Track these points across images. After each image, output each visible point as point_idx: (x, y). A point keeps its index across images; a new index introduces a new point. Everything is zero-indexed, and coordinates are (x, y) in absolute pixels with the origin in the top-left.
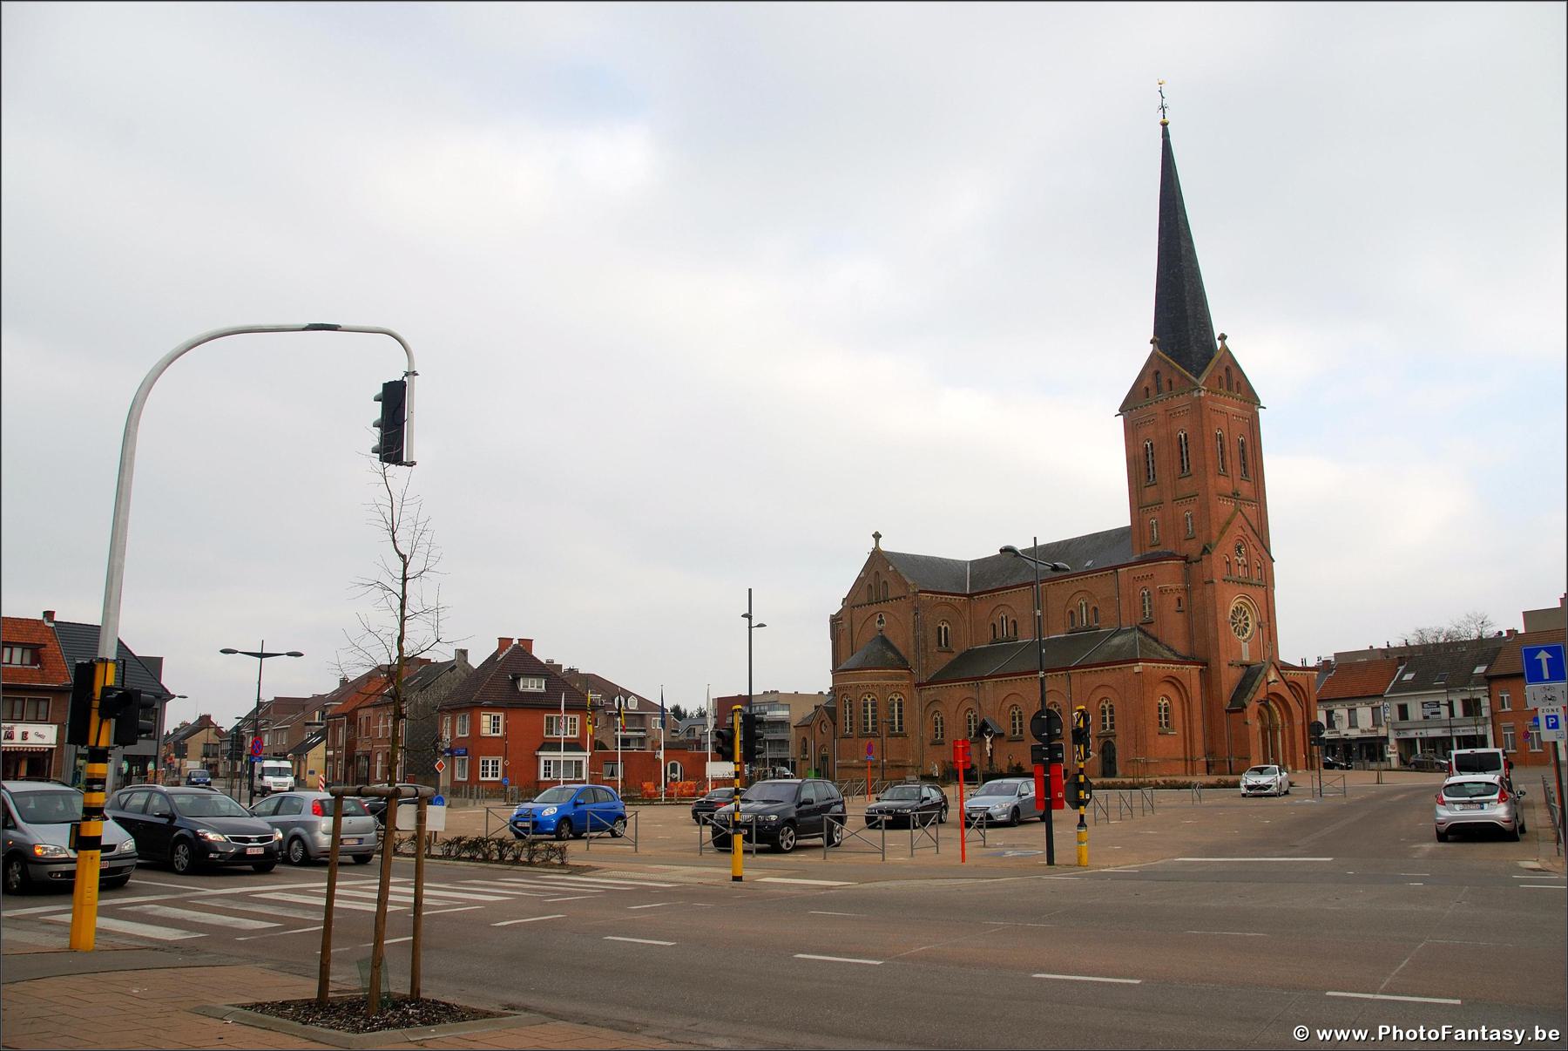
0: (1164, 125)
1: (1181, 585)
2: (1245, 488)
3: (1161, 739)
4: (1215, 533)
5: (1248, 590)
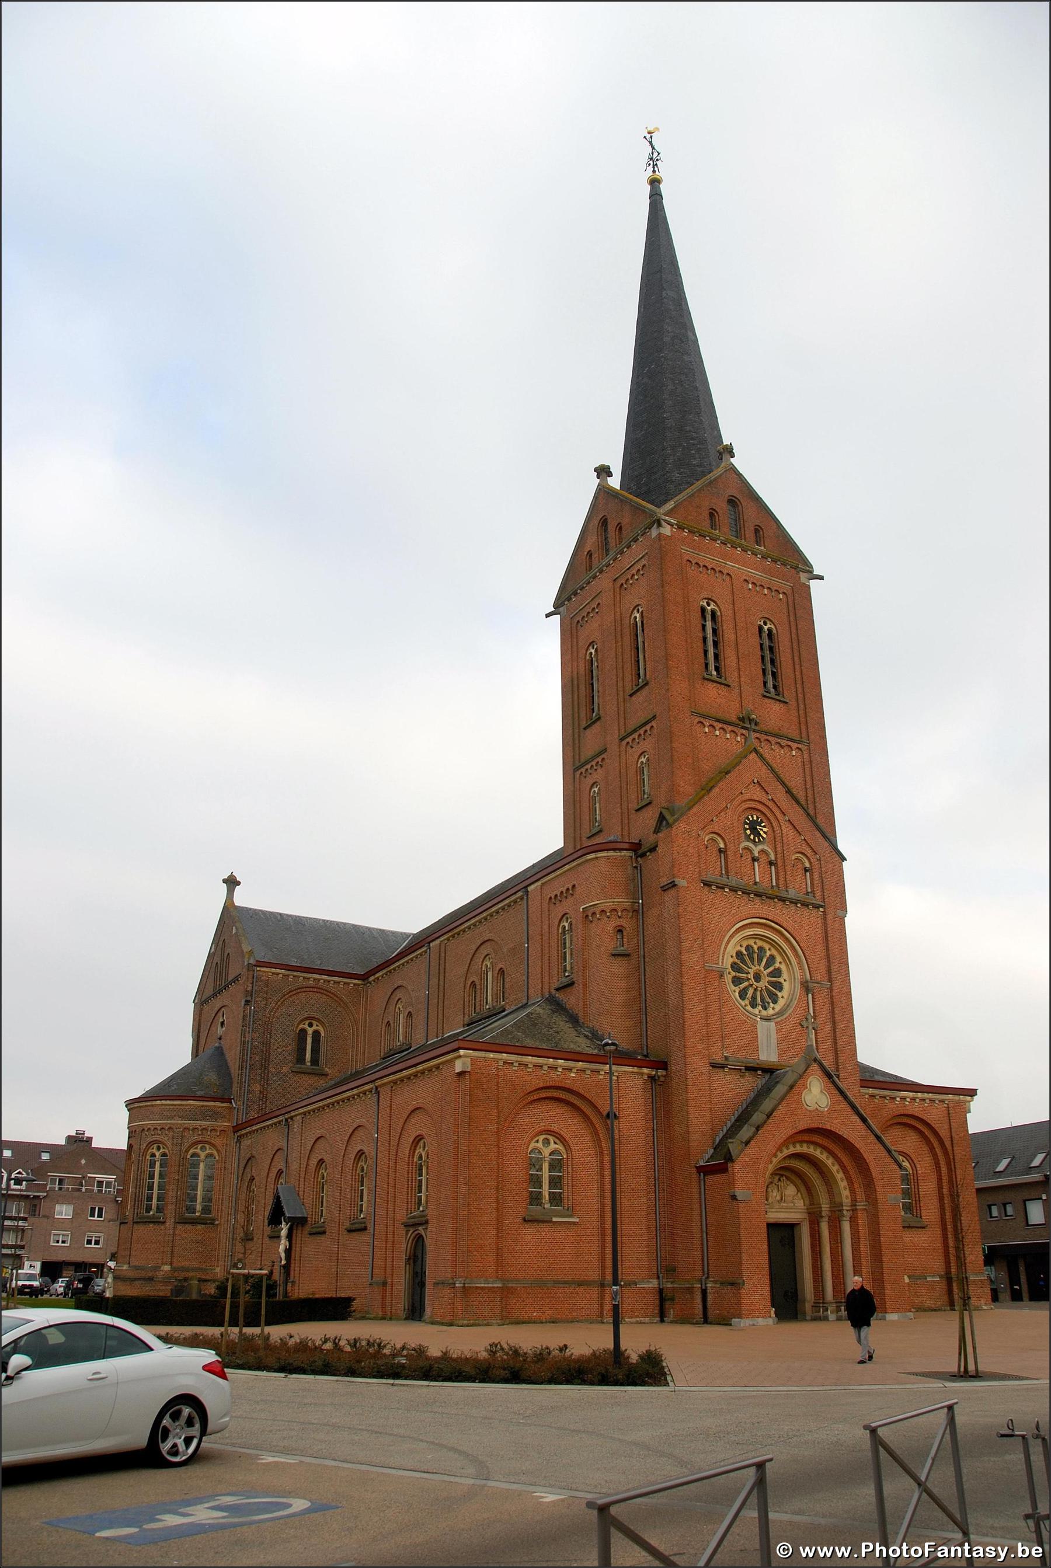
0: (655, 183)
1: (624, 902)
2: (772, 714)
3: (531, 1234)
4: (686, 786)
5: (774, 910)
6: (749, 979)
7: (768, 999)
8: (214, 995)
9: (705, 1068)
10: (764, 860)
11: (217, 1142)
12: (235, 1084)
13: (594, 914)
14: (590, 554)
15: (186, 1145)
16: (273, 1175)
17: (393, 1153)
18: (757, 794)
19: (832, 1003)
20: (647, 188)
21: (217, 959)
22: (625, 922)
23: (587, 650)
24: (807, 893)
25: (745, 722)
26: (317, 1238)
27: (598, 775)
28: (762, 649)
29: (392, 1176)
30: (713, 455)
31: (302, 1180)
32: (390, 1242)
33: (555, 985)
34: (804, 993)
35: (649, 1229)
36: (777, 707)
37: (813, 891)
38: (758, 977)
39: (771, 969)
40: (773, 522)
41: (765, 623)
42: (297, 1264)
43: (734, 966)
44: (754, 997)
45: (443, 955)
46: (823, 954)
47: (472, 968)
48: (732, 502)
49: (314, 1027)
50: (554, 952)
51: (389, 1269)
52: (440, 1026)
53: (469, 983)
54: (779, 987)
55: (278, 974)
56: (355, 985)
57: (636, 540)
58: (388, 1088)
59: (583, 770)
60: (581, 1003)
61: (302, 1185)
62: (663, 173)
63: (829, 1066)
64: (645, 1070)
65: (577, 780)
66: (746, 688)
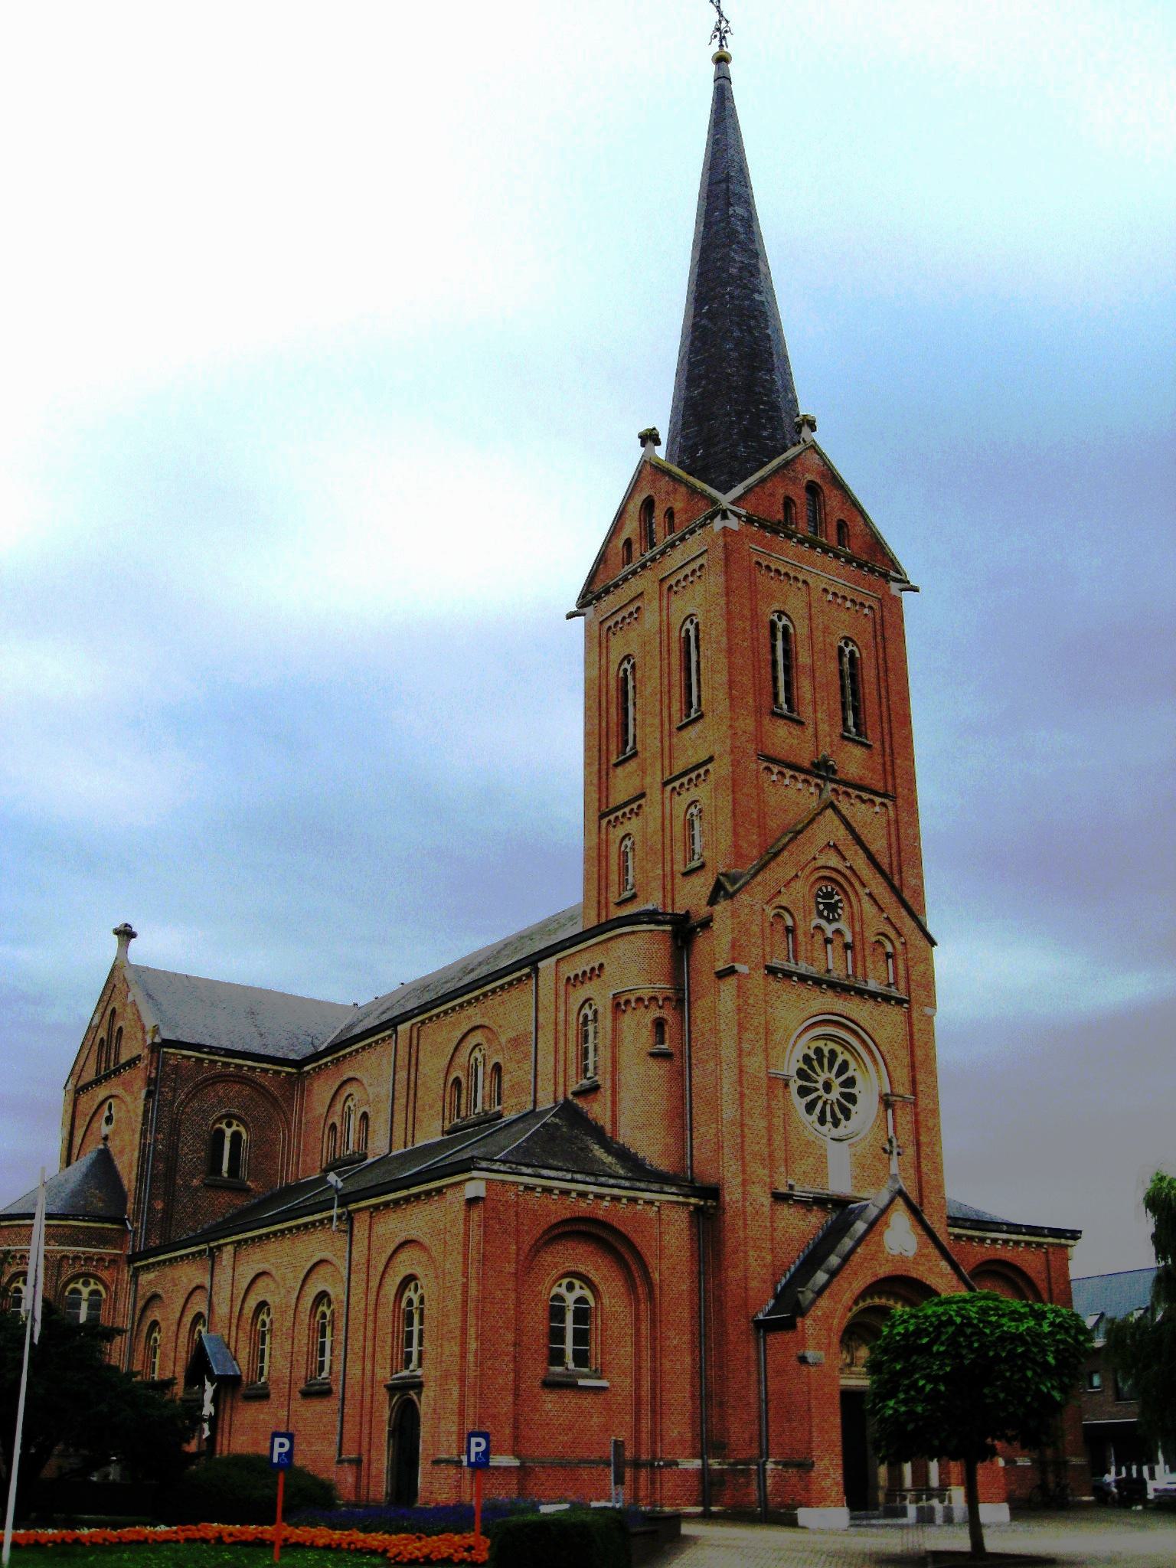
0: (721, 60)
2: (853, 762)
3: (551, 1403)
6: (817, 1090)
7: (840, 1116)
8: (97, 1082)
9: (767, 1201)
10: (838, 942)
11: (104, 1274)
12: (131, 1199)
13: (628, 1002)
14: (628, 543)
15: (64, 1278)
16: (188, 1319)
17: (372, 1297)
18: (834, 861)
19: (917, 1122)
20: (711, 69)
21: (102, 1033)
22: (667, 1014)
23: (621, 664)
24: (889, 985)
25: (822, 770)
26: (256, 1405)
27: (632, 825)
28: (842, 677)
29: (371, 1325)
30: (787, 428)
31: (234, 1328)
32: (366, 1410)
33: (575, 1088)
34: (882, 1108)
35: (693, 1396)
36: (858, 752)
37: (896, 983)
38: (828, 1087)
39: (843, 1078)
40: (859, 518)
41: (847, 645)
42: (226, 1435)
43: (801, 1074)
44: (823, 1112)
45: (415, 1042)
46: (907, 1060)
47: (457, 1061)
48: (812, 489)
49: (234, 1128)
50: (572, 1049)
51: (365, 1445)
52: (410, 1133)
53: (451, 1080)
54: (852, 1099)
55: (189, 1057)
56: (288, 1073)
57: (692, 532)
58: (365, 1216)
59: (612, 817)
60: (609, 1113)
61: (233, 1333)
62: (732, 47)
63: (915, 1200)
64: (692, 1200)
65: (603, 831)
66: (824, 728)
